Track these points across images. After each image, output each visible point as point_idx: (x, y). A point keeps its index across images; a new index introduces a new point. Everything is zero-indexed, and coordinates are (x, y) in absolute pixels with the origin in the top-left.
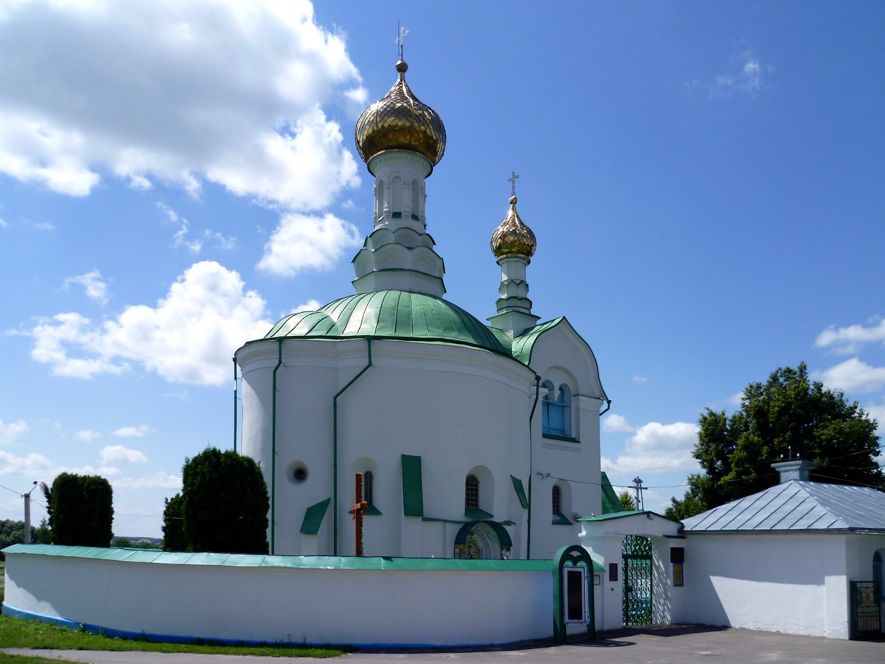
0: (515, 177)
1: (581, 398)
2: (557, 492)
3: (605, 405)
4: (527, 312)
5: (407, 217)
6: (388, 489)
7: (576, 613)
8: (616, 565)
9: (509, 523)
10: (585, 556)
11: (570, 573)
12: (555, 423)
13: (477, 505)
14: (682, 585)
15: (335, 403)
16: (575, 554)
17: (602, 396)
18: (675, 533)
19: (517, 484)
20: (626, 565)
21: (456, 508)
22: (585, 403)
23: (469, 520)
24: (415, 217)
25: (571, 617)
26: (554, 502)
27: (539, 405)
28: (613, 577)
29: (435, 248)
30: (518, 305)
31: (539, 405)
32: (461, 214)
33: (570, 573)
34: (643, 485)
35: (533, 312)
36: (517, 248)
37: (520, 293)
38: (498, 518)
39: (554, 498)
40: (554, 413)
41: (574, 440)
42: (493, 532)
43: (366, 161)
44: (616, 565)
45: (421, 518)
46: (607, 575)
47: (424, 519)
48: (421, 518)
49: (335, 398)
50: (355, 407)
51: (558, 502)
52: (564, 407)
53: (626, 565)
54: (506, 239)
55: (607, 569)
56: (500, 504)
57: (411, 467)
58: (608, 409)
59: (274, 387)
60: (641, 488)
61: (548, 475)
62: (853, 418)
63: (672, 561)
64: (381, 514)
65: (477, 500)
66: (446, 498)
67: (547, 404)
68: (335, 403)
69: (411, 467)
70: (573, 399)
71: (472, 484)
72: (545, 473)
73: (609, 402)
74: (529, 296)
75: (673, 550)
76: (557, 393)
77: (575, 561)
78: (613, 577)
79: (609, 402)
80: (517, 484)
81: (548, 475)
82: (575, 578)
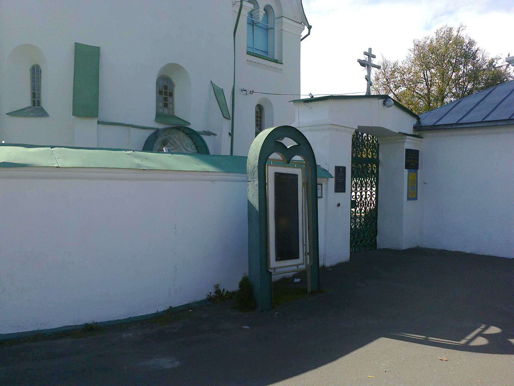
1: (283, 18)
2: (260, 110)
3: (306, 31)
6: (58, 90)
7: (288, 250)
8: (344, 168)
9: (209, 134)
10: (304, 146)
11: (278, 176)
12: (260, 44)
14: (416, 199)
16: (289, 143)
17: (304, 22)
18: (410, 130)
19: (218, 93)
22: (287, 25)
26: (257, 121)
33: (278, 176)
38: (196, 126)
39: (257, 117)
40: (259, 34)
42: (181, 134)
44: (344, 168)
45: (95, 121)
46: (332, 182)
48: (95, 121)
51: (261, 121)
55: (333, 172)
57: (87, 61)
58: (309, 34)
61: (252, 92)
62: (484, 70)
63: (407, 167)
66: (131, 97)
67: (252, 24)
69: (87, 61)
70: (277, 21)
71: (165, 91)
73: (310, 28)
75: (408, 152)
76: (262, 13)
77: (288, 154)
80: (218, 93)
81: (252, 92)
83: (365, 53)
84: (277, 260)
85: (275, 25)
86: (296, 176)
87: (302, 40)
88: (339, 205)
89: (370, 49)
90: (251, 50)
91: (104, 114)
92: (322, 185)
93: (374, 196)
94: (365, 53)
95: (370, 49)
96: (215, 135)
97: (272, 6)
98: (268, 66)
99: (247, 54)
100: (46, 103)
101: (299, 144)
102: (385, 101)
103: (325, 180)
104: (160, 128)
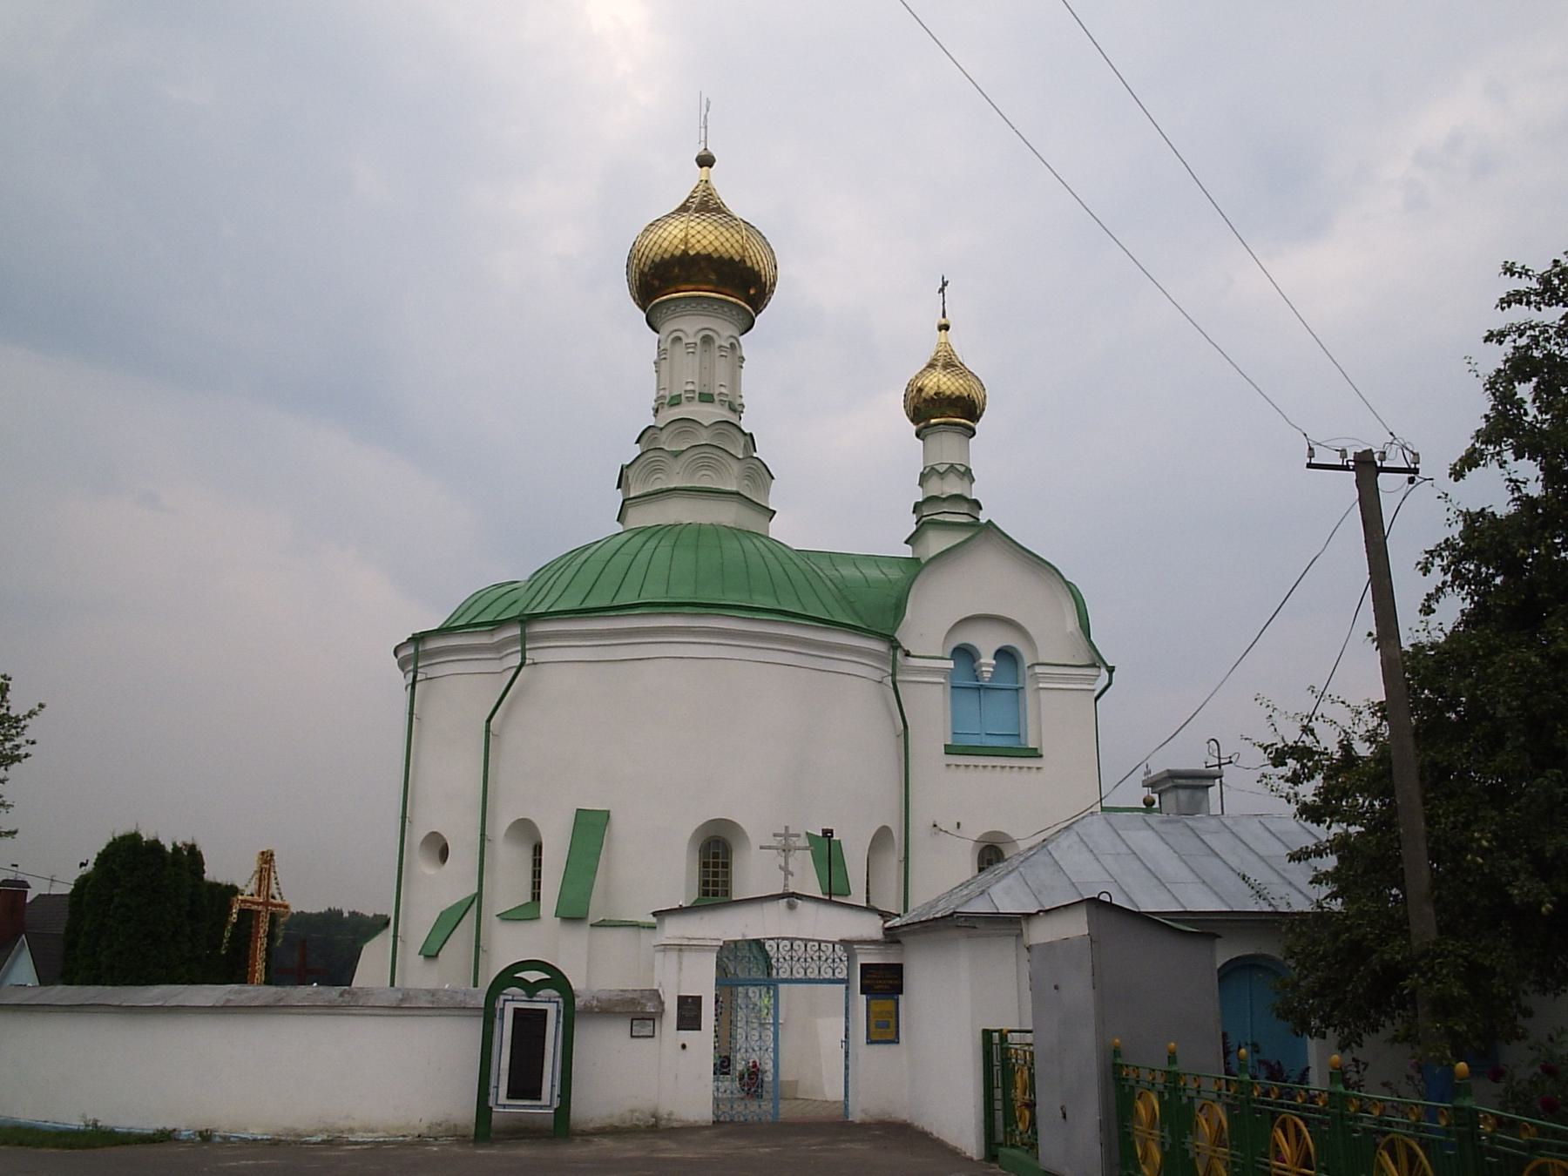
5: (690, 399)
13: (727, 893)
15: (488, 731)
37: (952, 487)
41: (1035, 754)
44: (697, 1001)
69: (591, 828)
73: (1111, 670)
82: (529, 1026)
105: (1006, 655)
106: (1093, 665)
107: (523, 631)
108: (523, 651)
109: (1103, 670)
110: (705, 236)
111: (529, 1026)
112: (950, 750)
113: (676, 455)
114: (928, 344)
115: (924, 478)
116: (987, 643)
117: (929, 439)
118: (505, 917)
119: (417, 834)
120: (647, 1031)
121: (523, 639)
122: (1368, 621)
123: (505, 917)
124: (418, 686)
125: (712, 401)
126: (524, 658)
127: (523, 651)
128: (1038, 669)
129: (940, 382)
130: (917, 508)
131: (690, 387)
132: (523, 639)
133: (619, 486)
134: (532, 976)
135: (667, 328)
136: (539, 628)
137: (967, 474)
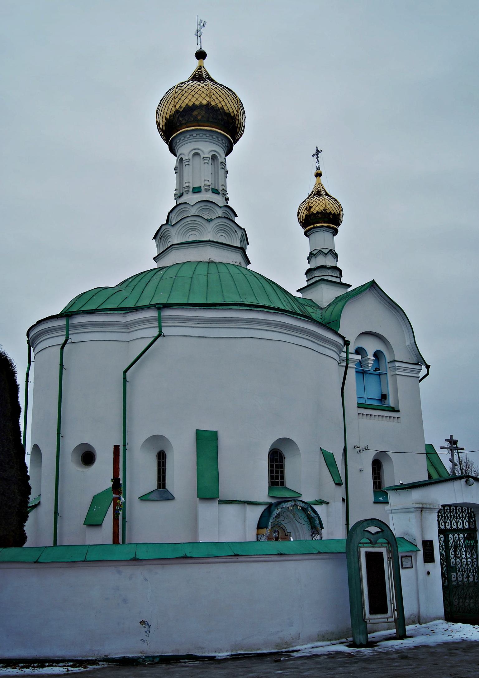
0: (317, 153)
2: (377, 466)
4: (337, 280)
5: (207, 190)
9: (321, 502)
11: (368, 554)
13: (283, 484)
15: (125, 378)
19: (329, 460)
20: (446, 541)
21: (261, 491)
23: (273, 501)
24: (215, 191)
25: (373, 611)
27: (352, 373)
28: (429, 558)
29: (236, 220)
30: (323, 271)
31: (352, 373)
32: (262, 184)
33: (368, 554)
34: (459, 445)
35: (344, 280)
36: (321, 219)
37: (329, 261)
38: (307, 497)
41: (393, 410)
43: (167, 143)
44: (431, 542)
46: (420, 555)
47: (221, 502)
49: (125, 372)
50: (144, 380)
52: (379, 375)
53: (446, 541)
54: (312, 210)
55: (420, 546)
56: (306, 478)
57: (207, 442)
58: (428, 374)
59: (61, 365)
60: (458, 449)
64: (173, 498)
65: (282, 478)
67: (362, 373)
68: (125, 378)
69: (207, 442)
71: (276, 459)
72: (362, 446)
73: (428, 367)
74: (339, 265)
78: (429, 558)
79: (428, 367)
82: (374, 560)
83: (447, 440)
84: (371, 613)
85: (388, 370)
86: (381, 554)
87: (420, 381)
88: (429, 573)
89: (451, 436)
90: (362, 401)
91: (225, 492)
92: (411, 557)
93: (476, 563)
94: (447, 440)
95: (451, 436)
96: (328, 503)
97: (382, 350)
98: (382, 416)
99: (358, 407)
100: (172, 484)
101: (382, 531)
102: (466, 481)
103: (414, 553)
104: (273, 502)
105: (378, 355)
106: (417, 364)
107: (67, 322)
108: (160, 327)
109: (424, 367)
110: (200, 95)
111: (374, 560)
112: (375, 503)
113: (209, 221)
114: (310, 185)
115: (309, 259)
116: (371, 346)
117: (312, 236)
118: (144, 498)
119: (71, 444)
120: (409, 565)
121: (67, 327)
122: (128, 384)
123: (144, 498)
124: (67, 346)
125: (219, 194)
126: (160, 331)
127: (160, 327)
128: (397, 364)
129: (318, 206)
130: (308, 272)
131: (207, 183)
132: (67, 327)
133: (155, 238)
134: (373, 529)
135: (185, 150)
136: (167, 313)
137: (336, 256)
